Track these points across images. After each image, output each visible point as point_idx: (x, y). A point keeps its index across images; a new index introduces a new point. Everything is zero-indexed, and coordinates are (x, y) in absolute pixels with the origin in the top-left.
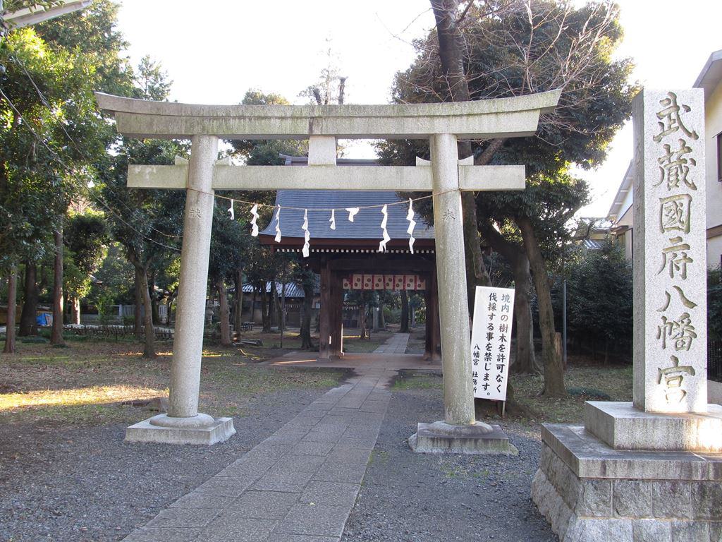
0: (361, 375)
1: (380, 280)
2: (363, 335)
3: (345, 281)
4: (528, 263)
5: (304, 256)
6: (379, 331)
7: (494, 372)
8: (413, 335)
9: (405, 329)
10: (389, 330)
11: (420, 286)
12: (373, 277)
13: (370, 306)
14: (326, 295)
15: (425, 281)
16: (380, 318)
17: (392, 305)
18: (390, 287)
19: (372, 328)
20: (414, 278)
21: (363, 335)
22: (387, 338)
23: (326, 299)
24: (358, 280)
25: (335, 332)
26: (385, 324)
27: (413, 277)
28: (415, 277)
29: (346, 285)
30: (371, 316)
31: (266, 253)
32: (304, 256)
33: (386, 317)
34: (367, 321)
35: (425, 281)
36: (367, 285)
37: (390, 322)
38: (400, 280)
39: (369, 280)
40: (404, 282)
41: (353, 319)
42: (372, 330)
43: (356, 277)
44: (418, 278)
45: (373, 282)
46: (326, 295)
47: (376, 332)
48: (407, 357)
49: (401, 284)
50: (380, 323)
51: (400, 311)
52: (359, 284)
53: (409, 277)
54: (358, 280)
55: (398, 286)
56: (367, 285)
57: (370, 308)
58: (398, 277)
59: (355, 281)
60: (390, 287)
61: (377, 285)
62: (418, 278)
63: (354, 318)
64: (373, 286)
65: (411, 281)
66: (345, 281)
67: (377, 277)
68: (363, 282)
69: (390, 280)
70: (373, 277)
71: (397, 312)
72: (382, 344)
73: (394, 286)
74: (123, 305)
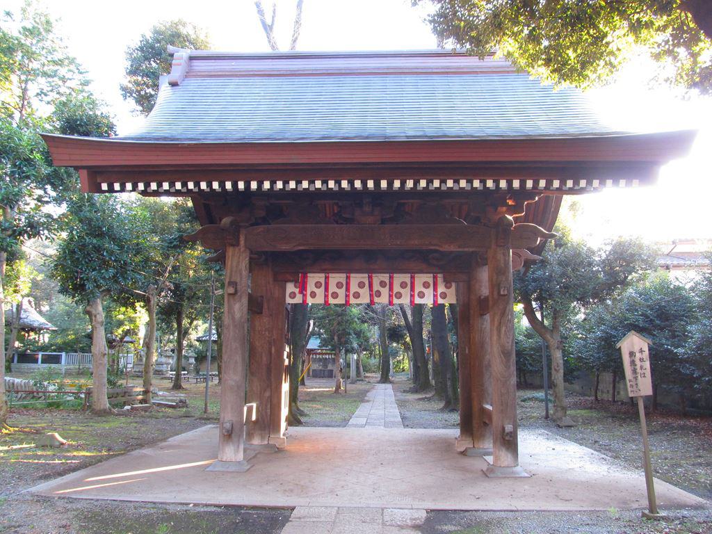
1: (361, 285)
2: (338, 387)
3: (290, 288)
6: (356, 381)
8: (396, 385)
9: (385, 379)
11: (444, 296)
13: (347, 351)
14: (237, 307)
16: (358, 368)
17: (371, 354)
18: (384, 299)
19: (349, 377)
20: (431, 281)
21: (338, 387)
22: (368, 391)
24: (318, 285)
25: (267, 394)
27: (428, 278)
28: (435, 278)
29: (293, 295)
30: (348, 365)
31: (195, 271)
33: (365, 367)
35: (454, 285)
36: (335, 295)
37: (367, 371)
38: (403, 285)
39: (339, 285)
40: (412, 289)
41: (328, 368)
42: (349, 381)
43: (313, 279)
44: (440, 280)
45: (348, 289)
46: (237, 307)
47: (353, 383)
48: (417, 442)
49: (406, 292)
50: (358, 373)
51: (377, 360)
52: (320, 292)
53: (421, 279)
54: (318, 285)
55: (399, 296)
56: (335, 295)
57: (346, 355)
58: (399, 278)
59: (311, 287)
60: (384, 299)
62: (440, 280)
63: (330, 367)
64: (347, 296)
65: (426, 285)
66: (290, 288)
67: (356, 279)
68: (327, 289)
69: (383, 284)
71: (374, 361)
72: (363, 401)
73: (391, 296)
74: (67, 352)
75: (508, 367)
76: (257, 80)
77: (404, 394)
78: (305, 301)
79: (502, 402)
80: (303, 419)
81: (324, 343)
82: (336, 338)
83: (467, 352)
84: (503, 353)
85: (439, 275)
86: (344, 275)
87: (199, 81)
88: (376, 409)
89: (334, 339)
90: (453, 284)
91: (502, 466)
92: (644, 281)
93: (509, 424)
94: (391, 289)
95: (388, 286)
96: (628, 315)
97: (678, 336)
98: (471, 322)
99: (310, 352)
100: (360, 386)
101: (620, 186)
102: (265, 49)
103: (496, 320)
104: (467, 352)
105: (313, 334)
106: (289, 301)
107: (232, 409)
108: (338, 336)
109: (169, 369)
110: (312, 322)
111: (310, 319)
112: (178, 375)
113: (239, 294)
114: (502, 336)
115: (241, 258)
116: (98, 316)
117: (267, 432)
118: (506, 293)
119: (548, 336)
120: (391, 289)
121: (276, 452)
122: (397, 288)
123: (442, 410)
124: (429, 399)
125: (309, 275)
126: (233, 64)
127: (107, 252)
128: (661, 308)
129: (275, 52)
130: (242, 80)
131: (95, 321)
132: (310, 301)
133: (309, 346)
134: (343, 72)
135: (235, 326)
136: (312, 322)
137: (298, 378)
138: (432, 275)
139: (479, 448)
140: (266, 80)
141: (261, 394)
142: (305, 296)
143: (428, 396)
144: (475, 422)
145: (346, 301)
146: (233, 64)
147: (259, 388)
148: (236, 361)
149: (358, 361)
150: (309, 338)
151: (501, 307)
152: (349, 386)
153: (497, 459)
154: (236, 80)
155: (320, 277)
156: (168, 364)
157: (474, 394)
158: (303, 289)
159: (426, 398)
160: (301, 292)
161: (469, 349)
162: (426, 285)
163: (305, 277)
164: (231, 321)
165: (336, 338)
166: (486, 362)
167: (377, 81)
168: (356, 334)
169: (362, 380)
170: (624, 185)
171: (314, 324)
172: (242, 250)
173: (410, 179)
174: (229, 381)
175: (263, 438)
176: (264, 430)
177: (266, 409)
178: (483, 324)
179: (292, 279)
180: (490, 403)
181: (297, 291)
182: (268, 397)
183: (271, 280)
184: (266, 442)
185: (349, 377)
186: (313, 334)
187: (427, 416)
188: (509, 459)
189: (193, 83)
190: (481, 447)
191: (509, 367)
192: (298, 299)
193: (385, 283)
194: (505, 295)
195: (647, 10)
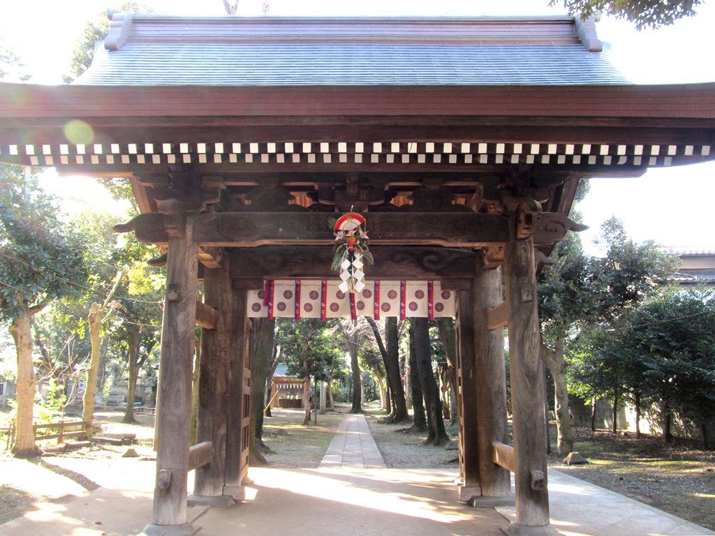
0: (275, 453)
4: (546, 201)
5: (362, 144)
7: (654, 463)
10: (338, 409)
12: (403, 286)
15: (452, 293)
19: (318, 408)
20: (425, 290)
23: (385, 346)
26: (364, 403)
27: (422, 286)
28: (430, 286)
30: (318, 394)
32: (362, 144)
34: (313, 399)
38: (392, 295)
39: (419, 294)
43: (282, 286)
47: (323, 413)
50: (328, 404)
59: (278, 297)
61: (414, 307)
66: (253, 298)
68: (403, 299)
70: (403, 286)
73: (376, 308)
75: (533, 394)
76: (214, 47)
77: (380, 425)
78: (270, 315)
79: (528, 440)
80: (267, 458)
81: (293, 370)
82: (305, 364)
83: (471, 376)
84: (527, 376)
85: (435, 282)
86: (319, 283)
87: (144, 46)
88: (352, 443)
89: (303, 366)
90: (452, 293)
91: (531, 524)
92: (651, 296)
93: (537, 468)
94: (377, 300)
95: (373, 297)
96: (639, 335)
97: (699, 357)
98: (476, 340)
99: (278, 381)
100: (329, 417)
101: (665, 164)
102: (221, 13)
103: (517, 334)
104: (471, 376)
105: (280, 360)
106: (251, 314)
107: (172, 453)
108: (308, 362)
109: (123, 399)
110: (279, 348)
111: (277, 345)
112: (130, 406)
113: (184, 301)
114: (526, 354)
115: (187, 253)
116: (24, 337)
117: (221, 479)
118: (530, 298)
119: (551, 359)
120: (377, 300)
121: (233, 506)
122: (384, 298)
123: (426, 443)
124: (407, 431)
125: (276, 282)
126: (186, 28)
127: (35, 261)
128: (677, 325)
129: (230, 16)
130: (196, 46)
131: (21, 343)
132: (276, 313)
133: (276, 374)
134: (320, 38)
135: (178, 343)
136: (279, 348)
137: (263, 408)
138: (426, 282)
139: (488, 497)
140: (225, 47)
141: (213, 431)
142: (271, 308)
143: (406, 427)
144: (483, 464)
145: (322, 314)
146: (186, 28)
147: (211, 423)
148: (179, 389)
149: (328, 389)
150: (276, 364)
151: (524, 317)
152: (318, 416)
153: (522, 514)
154: (189, 46)
155: (289, 284)
156: (122, 394)
157: (481, 429)
158: (268, 299)
159: (404, 429)
160: (266, 304)
161: (474, 373)
162: (419, 294)
163: (270, 285)
164: (172, 337)
165: (305, 364)
166: (494, 389)
167: (360, 50)
168: (326, 360)
169: (333, 410)
170: (670, 164)
171: (281, 350)
172: (188, 244)
173: (412, 142)
174: (169, 416)
175: (215, 488)
176: (218, 477)
177: (220, 450)
178: (491, 342)
179: (254, 286)
180: (500, 439)
181: (261, 301)
182: (223, 435)
183: (228, 287)
184: (220, 493)
185: (318, 408)
186: (280, 360)
187: (411, 451)
188: (539, 516)
189: (136, 49)
190: (492, 495)
191: (536, 394)
192: (262, 313)
193: (370, 292)
194: (528, 302)
195: (624, 14)
